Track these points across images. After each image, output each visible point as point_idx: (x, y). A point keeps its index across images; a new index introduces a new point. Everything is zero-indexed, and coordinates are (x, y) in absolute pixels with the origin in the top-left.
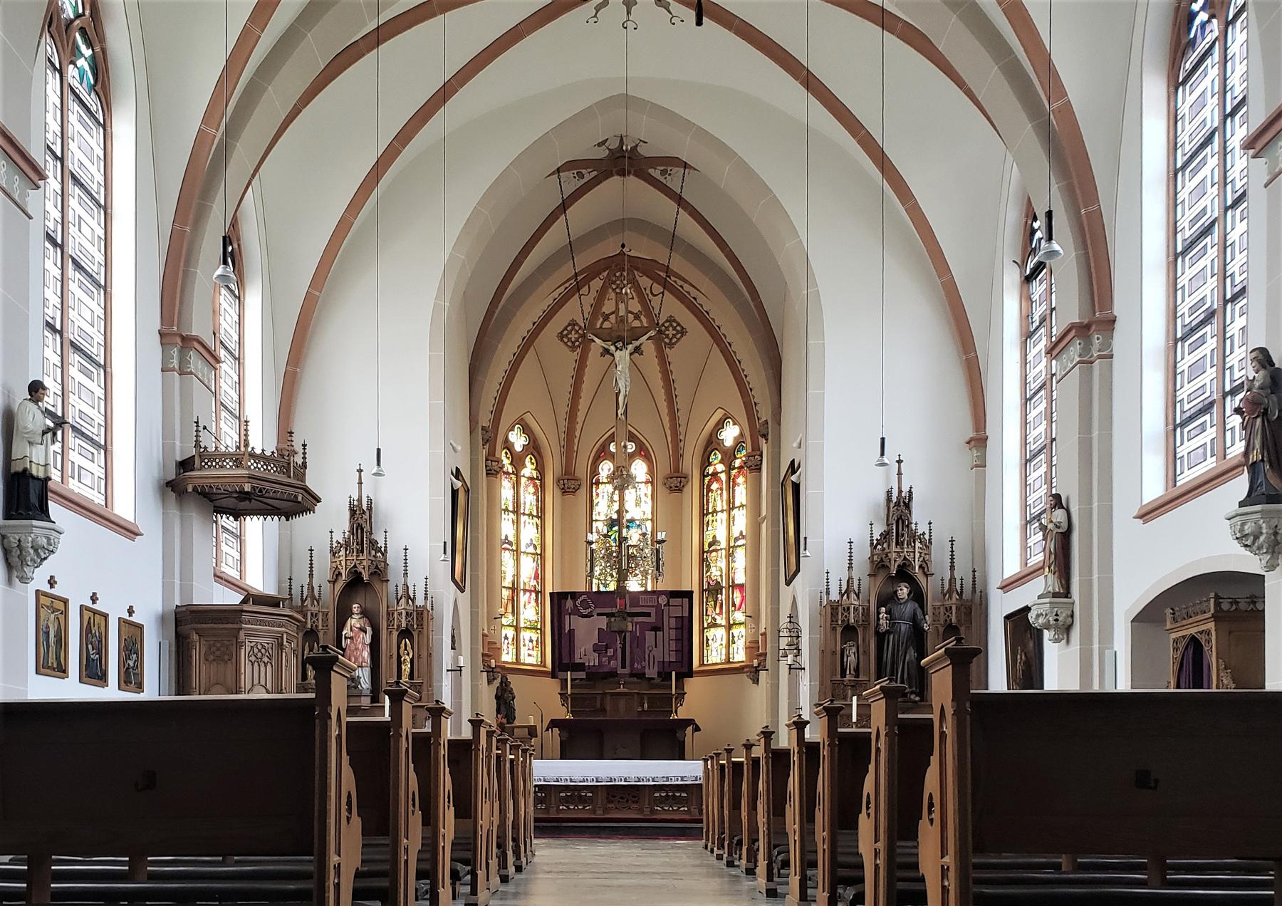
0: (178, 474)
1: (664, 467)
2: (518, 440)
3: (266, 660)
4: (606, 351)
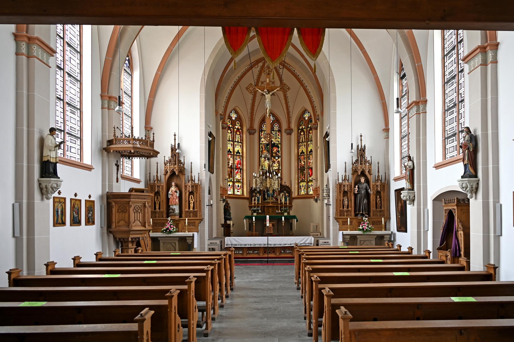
0: (107, 146)
1: (284, 126)
2: (234, 116)
3: (139, 211)
4: (263, 95)
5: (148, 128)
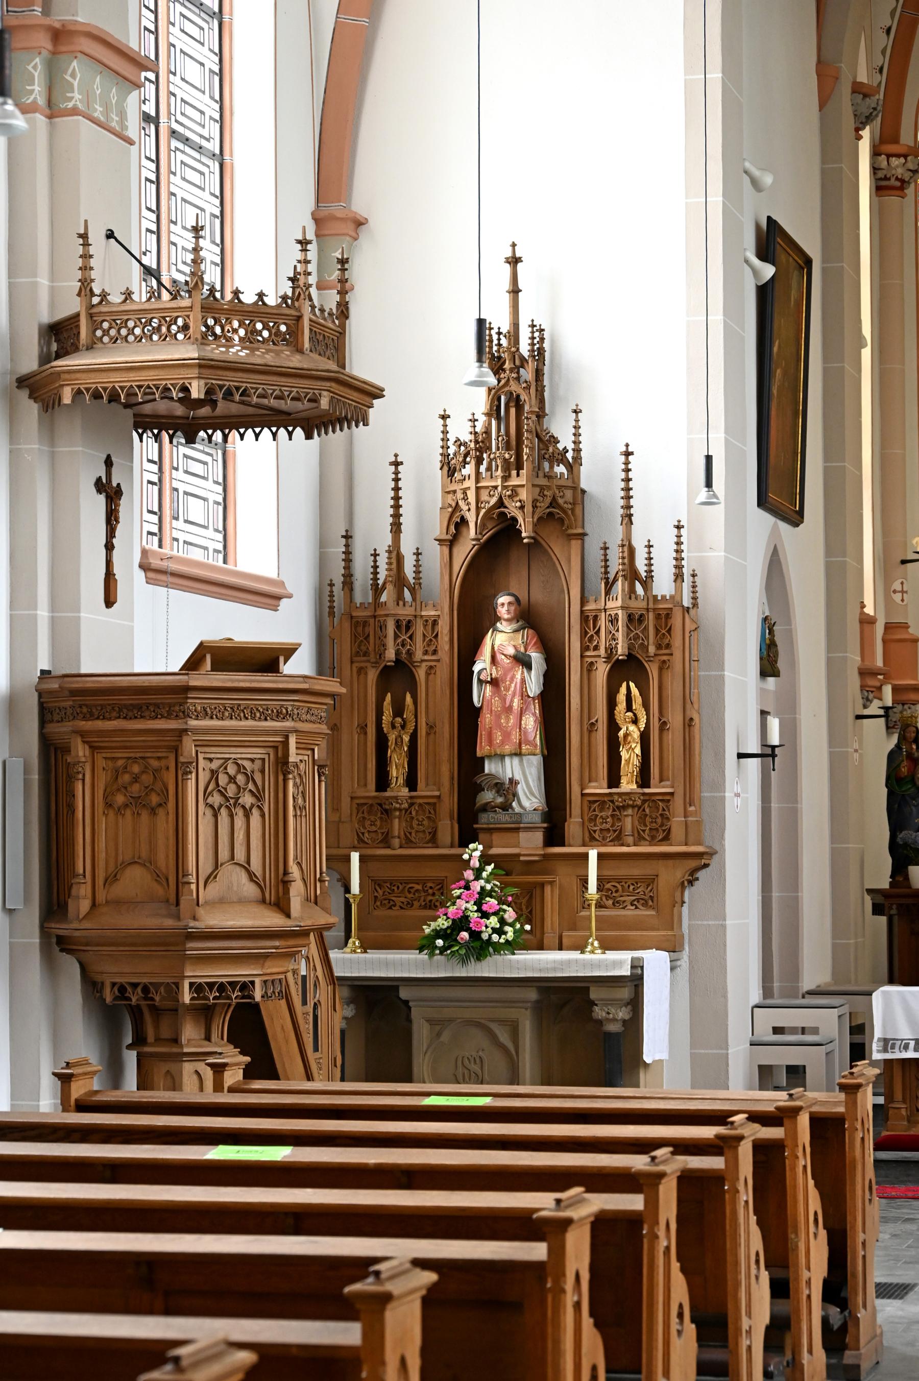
0: (45, 359)
3: (247, 800)
5: (334, 219)
